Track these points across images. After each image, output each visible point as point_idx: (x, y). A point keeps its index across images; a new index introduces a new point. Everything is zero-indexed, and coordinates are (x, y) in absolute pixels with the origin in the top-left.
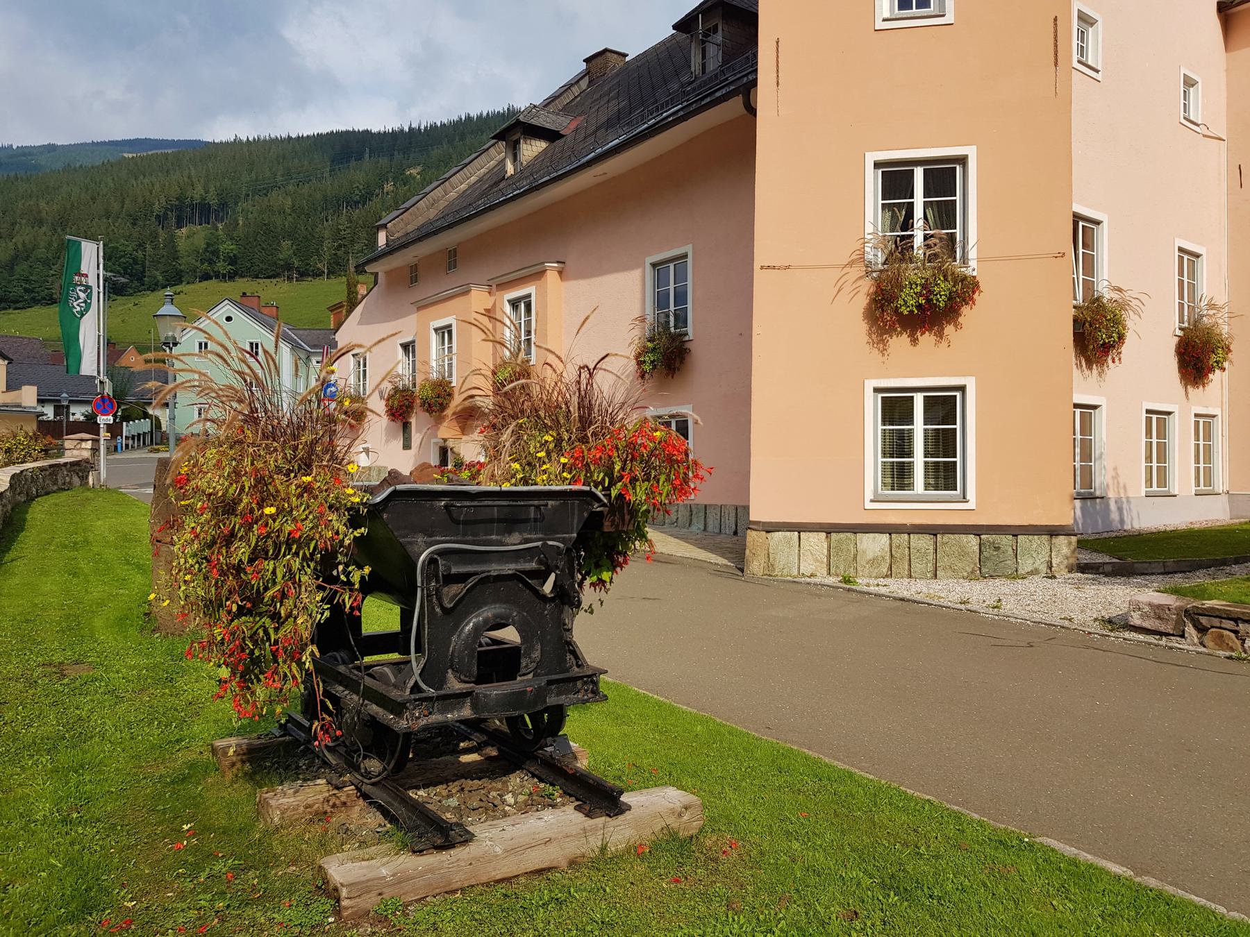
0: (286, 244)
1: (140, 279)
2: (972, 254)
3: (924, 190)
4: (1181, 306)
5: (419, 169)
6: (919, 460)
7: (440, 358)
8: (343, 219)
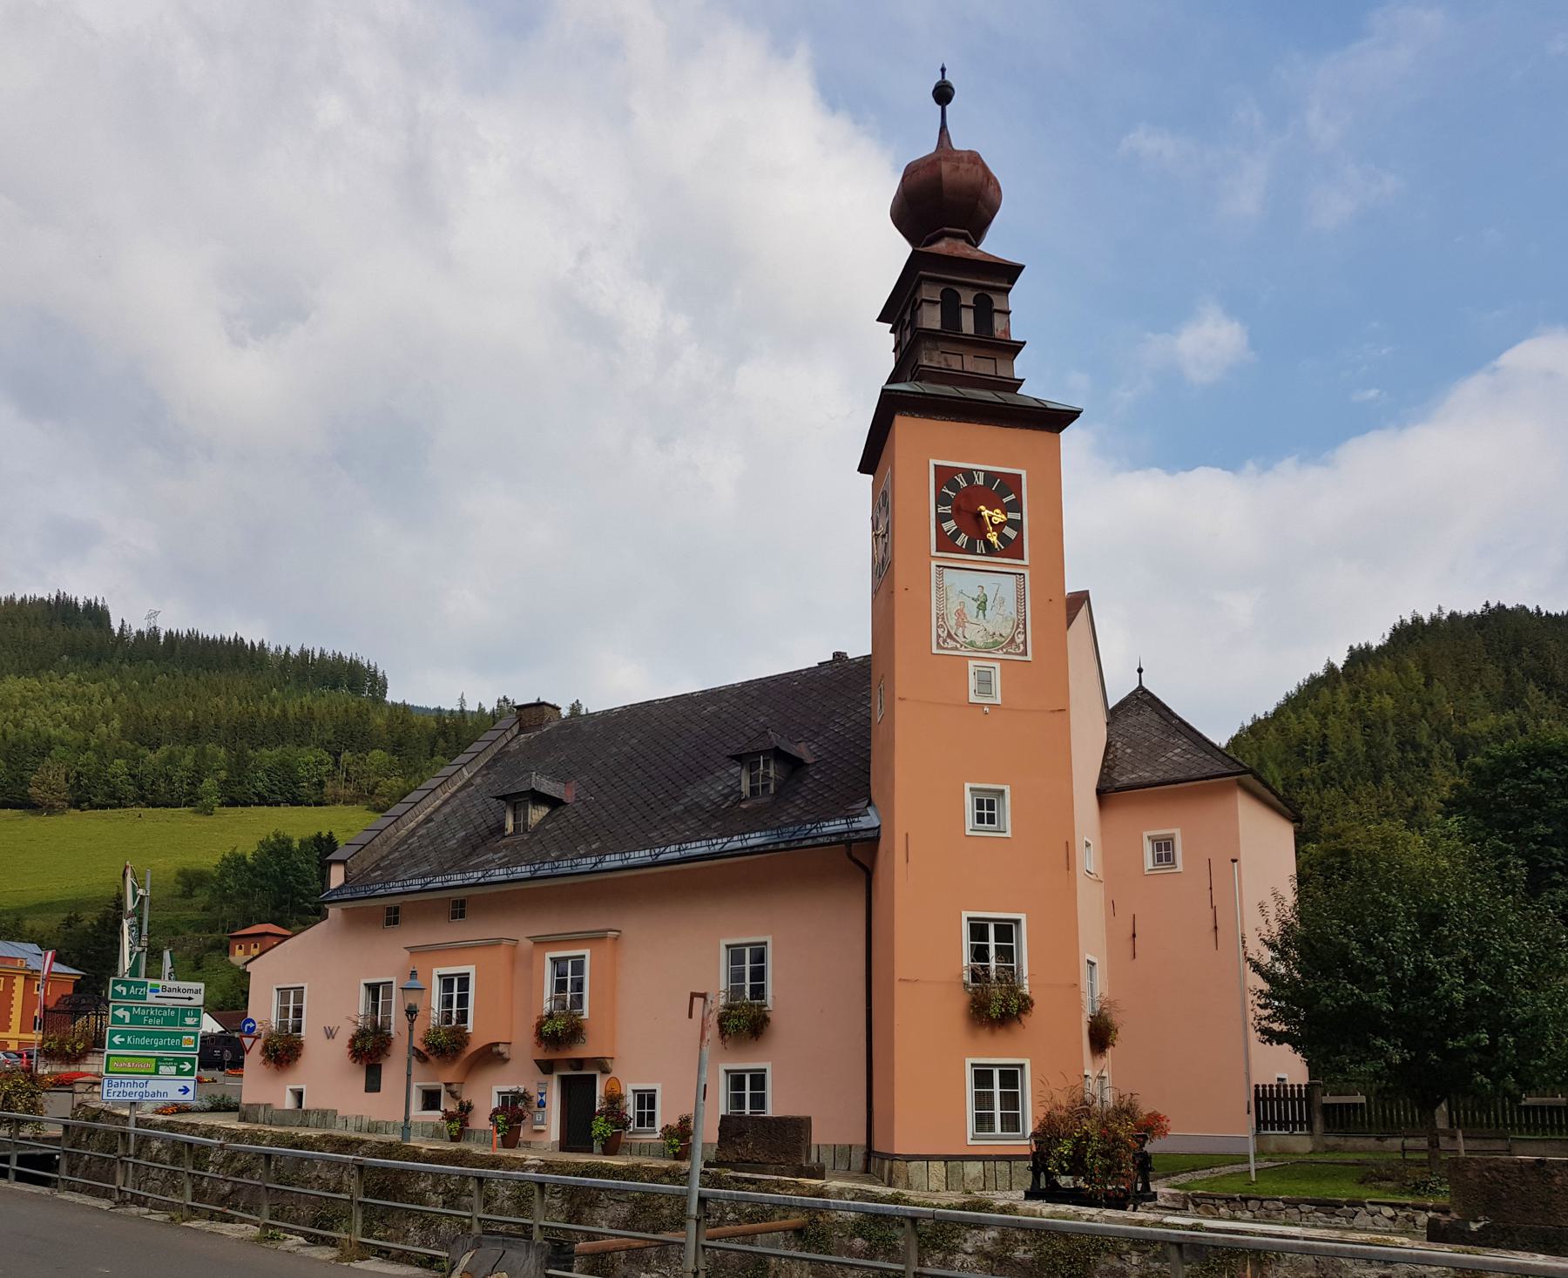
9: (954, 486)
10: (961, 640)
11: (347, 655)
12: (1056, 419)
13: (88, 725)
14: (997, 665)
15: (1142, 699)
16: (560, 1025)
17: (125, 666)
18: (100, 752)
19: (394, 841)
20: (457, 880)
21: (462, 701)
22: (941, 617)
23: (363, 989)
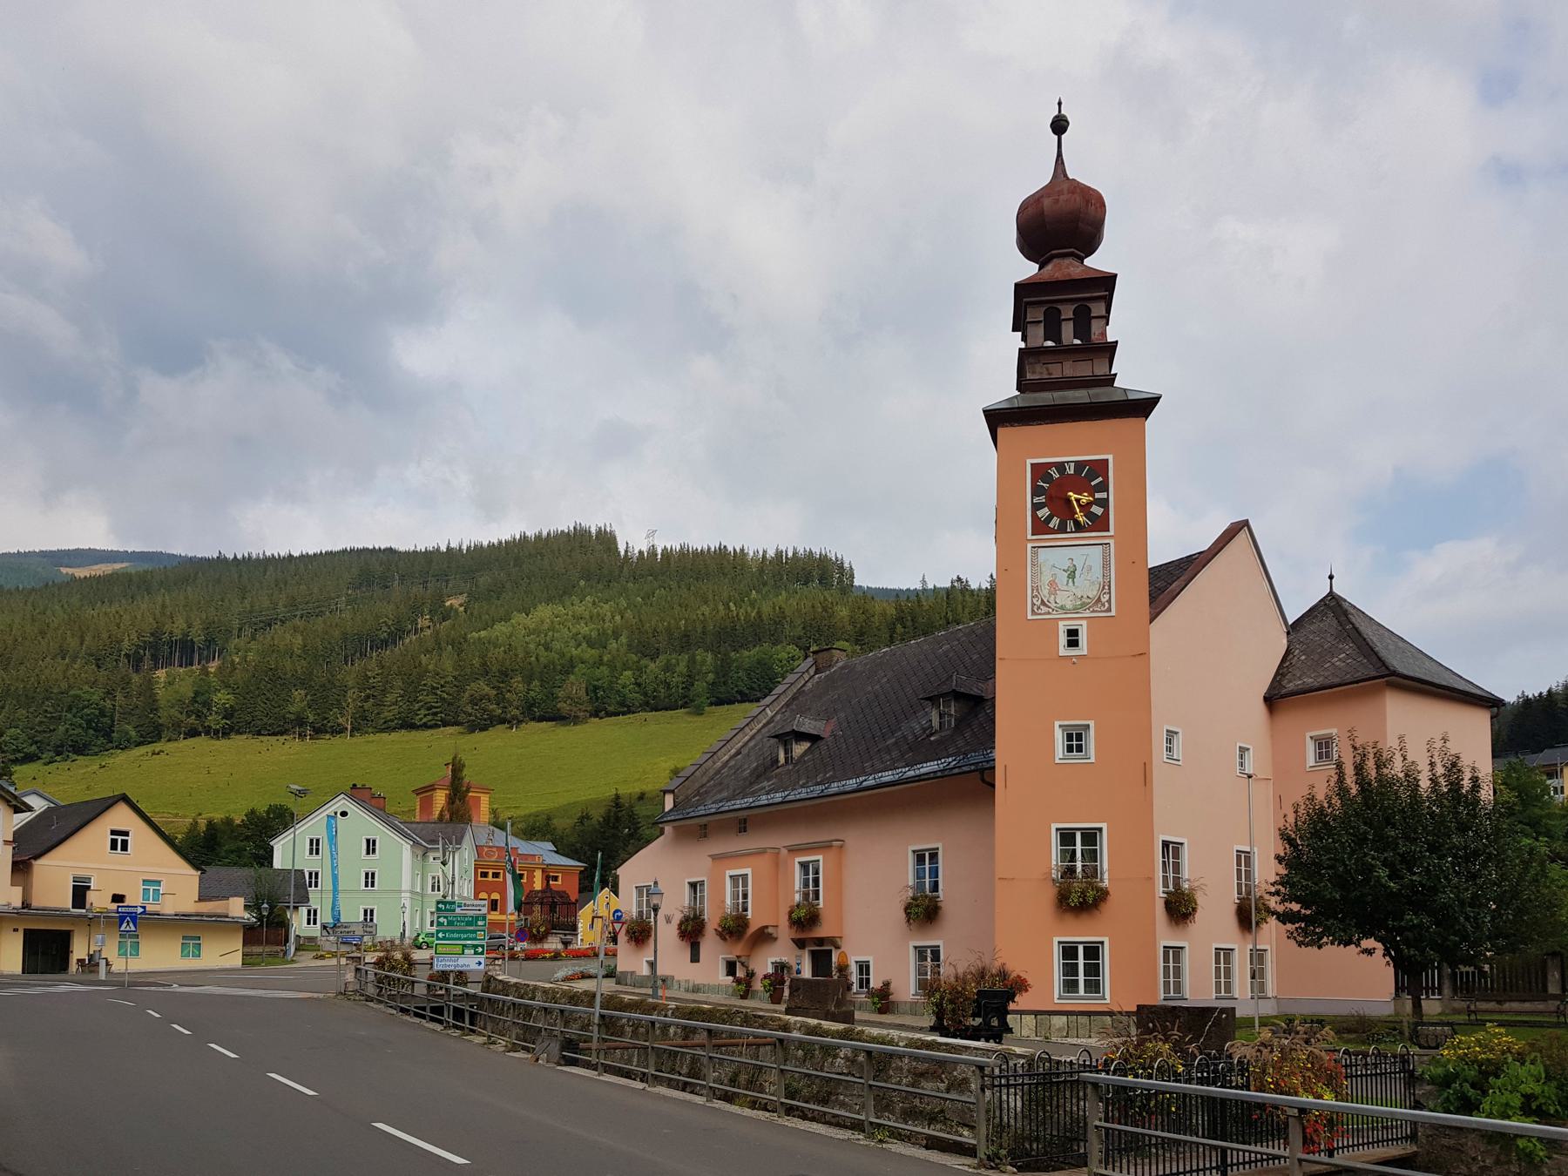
0: (298, 694)
1: (107, 733)
2: (1106, 876)
3: (1080, 843)
4: (1239, 885)
5: (462, 599)
6: (1081, 978)
7: (735, 896)
8: (373, 664)
9: (1047, 478)
10: (1053, 605)
11: (816, 551)
12: (1143, 407)
13: (598, 642)
14: (1084, 623)
15: (1332, 607)
16: (802, 913)
17: (630, 585)
18: (612, 666)
19: (712, 772)
20: (739, 804)
21: (924, 582)
22: (1036, 588)
23: (687, 886)
